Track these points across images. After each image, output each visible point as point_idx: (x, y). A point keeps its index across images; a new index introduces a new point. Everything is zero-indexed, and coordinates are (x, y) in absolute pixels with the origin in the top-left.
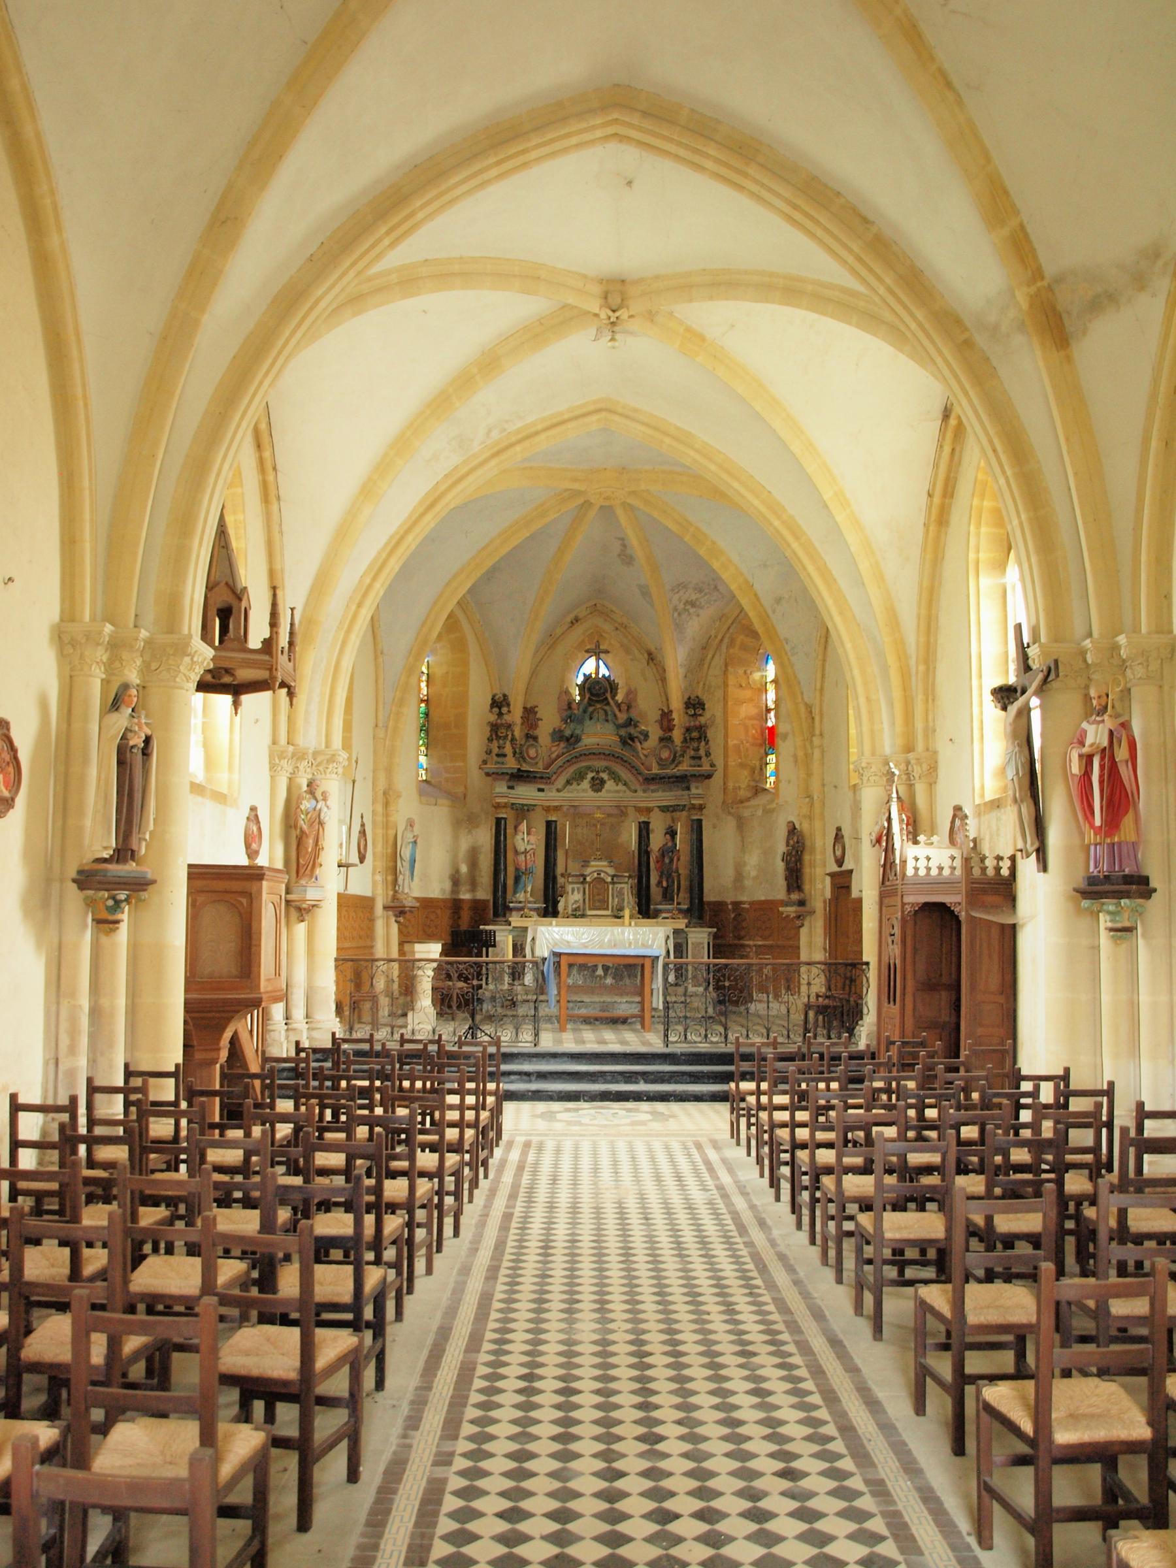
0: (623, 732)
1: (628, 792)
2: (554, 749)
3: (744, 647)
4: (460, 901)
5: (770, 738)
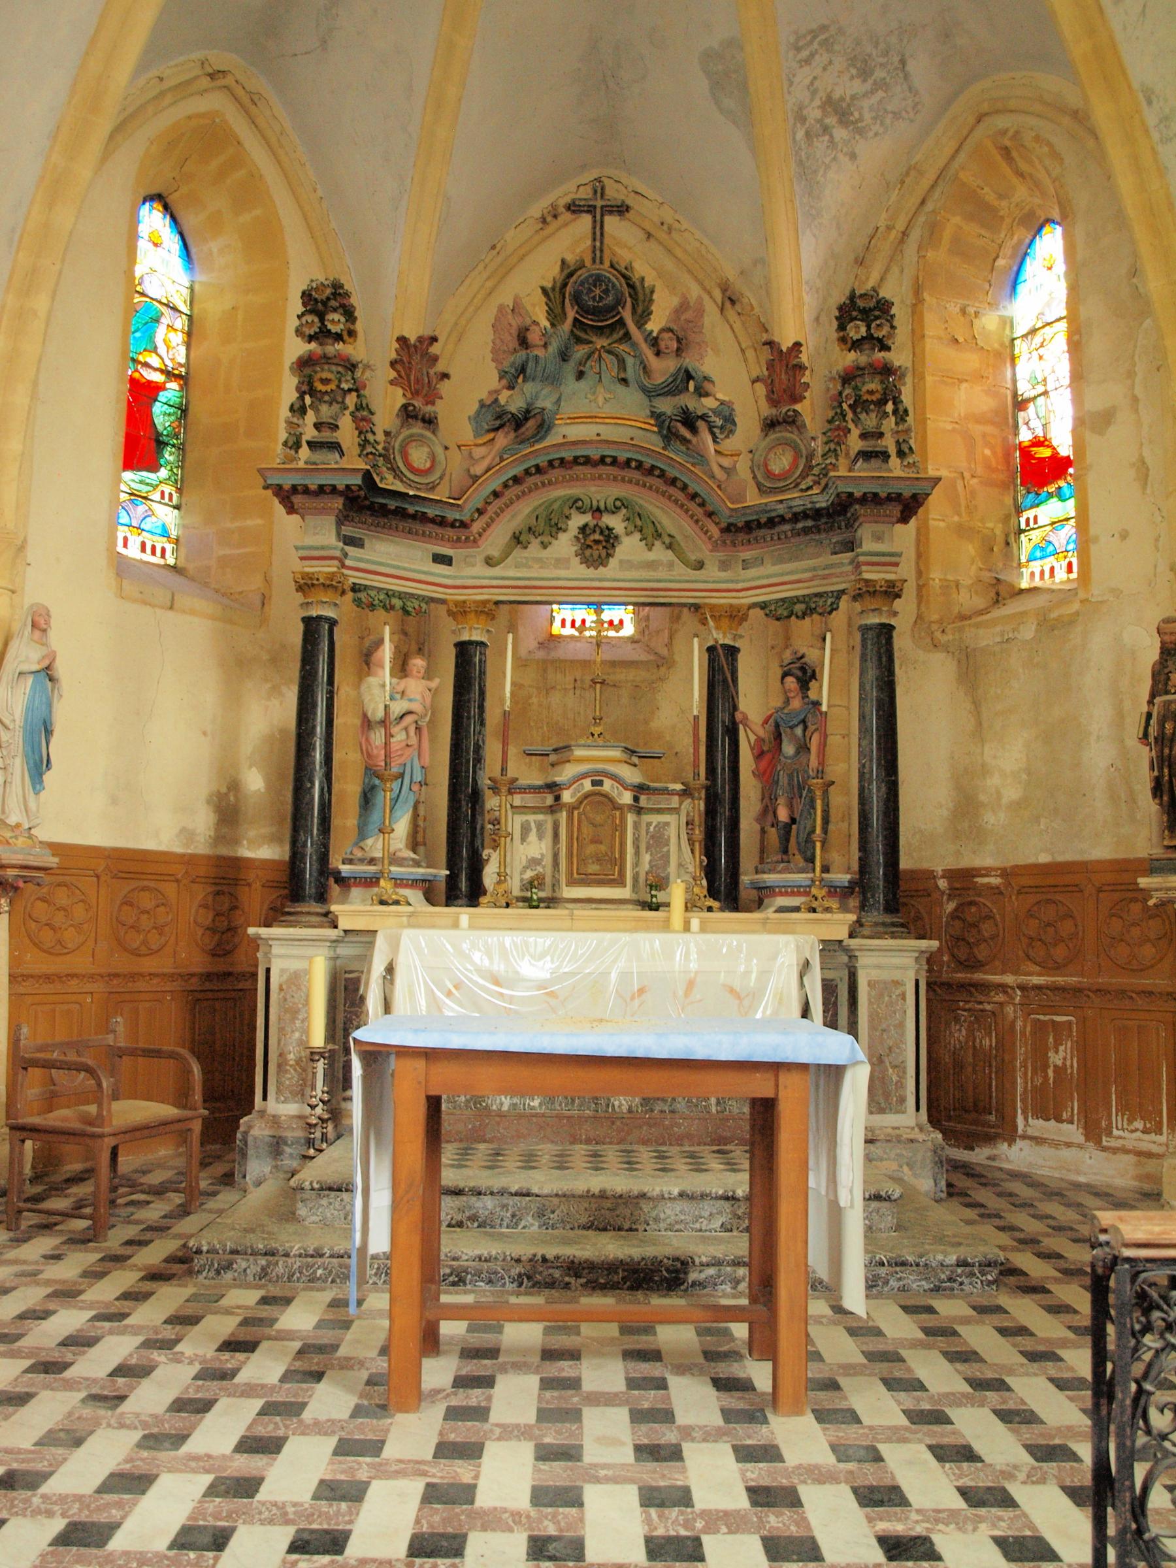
0: (666, 406)
1: (681, 570)
2: (478, 452)
3: (960, 249)
4: (237, 863)
5: (1041, 471)
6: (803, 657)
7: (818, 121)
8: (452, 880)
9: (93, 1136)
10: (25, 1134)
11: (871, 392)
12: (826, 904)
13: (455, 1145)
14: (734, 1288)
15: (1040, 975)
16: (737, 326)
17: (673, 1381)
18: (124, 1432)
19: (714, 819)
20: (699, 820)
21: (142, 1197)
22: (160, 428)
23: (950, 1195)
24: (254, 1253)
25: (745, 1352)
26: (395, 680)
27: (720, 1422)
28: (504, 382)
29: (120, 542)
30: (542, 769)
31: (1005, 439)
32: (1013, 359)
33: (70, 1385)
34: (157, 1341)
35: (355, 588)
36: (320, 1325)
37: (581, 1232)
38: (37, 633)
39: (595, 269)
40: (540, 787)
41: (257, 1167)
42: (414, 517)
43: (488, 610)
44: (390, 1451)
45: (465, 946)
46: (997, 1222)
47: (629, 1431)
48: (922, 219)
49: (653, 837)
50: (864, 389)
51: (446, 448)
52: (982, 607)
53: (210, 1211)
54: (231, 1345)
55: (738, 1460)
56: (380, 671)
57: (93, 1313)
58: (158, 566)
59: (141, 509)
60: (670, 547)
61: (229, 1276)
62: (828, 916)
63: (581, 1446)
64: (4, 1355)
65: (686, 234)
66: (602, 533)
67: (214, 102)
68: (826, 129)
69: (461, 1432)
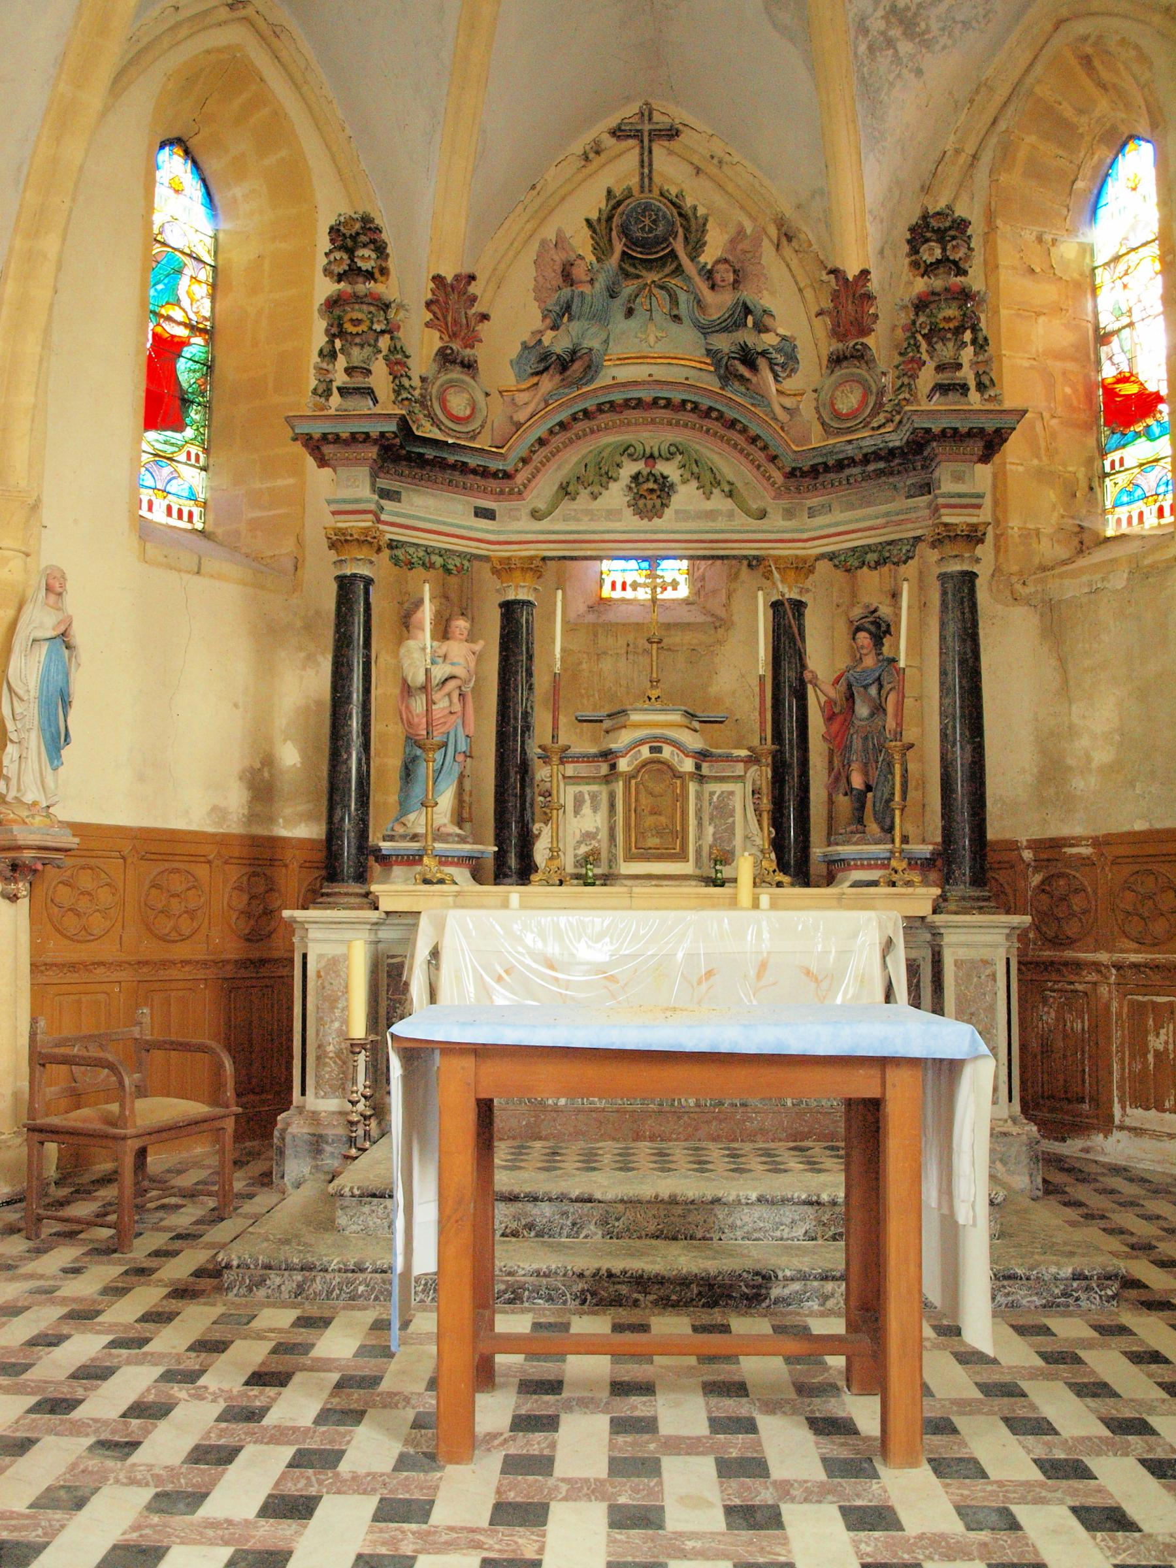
0: (723, 343)
1: (742, 521)
2: (522, 398)
3: (1037, 172)
4: (274, 842)
5: (1127, 409)
6: (875, 611)
7: (883, 33)
8: (500, 857)
9: (115, 1138)
10: (43, 1136)
11: (948, 320)
12: (907, 877)
13: (510, 1143)
14: (822, 1305)
15: (1137, 951)
16: (794, 264)
17: (764, 1422)
18: (134, 1489)
19: (782, 787)
20: (766, 788)
21: (173, 1200)
22: (185, 385)
23: (1047, 1192)
24: (289, 1268)
25: (842, 1383)
26: (436, 644)
27: (822, 1476)
28: (548, 321)
29: (145, 505)
30: (595, 740)
31: (1086, 377)
32: (1094, 290)
33: (78, 1429)
34: (179, 1372)
35: (393, 545)
36: (362, 1351)
37: (648, 1242)
38: (52, 598)
39: (644, 198)
40: (595, 756)
41: (296, 1167)
42: (453, 467)
43: (536, 567)
44: (440, 1516)
45: (517, 927)
46: (1103, 1223)
47: (717, 1488)
48: (993, 140)
49: (716, 808)
50: (940, 316)
51: (487, 394)
52: (1064, 557)
53: (246, 1216)
54: (258, 1379)
55: (850, 1528)
56: (420, 634)
57: (110, 1338)
58: (185, 530)
59: (167, 471)
60: (730, 495)
61: (261, 1293)
62: (910, 890)
63: (662, 1508)
64: (7, 1390)
65: (739, 168)
66: (655, 481)
67: (233, 35)
68: (890, 43)
69: (522, 1489)
